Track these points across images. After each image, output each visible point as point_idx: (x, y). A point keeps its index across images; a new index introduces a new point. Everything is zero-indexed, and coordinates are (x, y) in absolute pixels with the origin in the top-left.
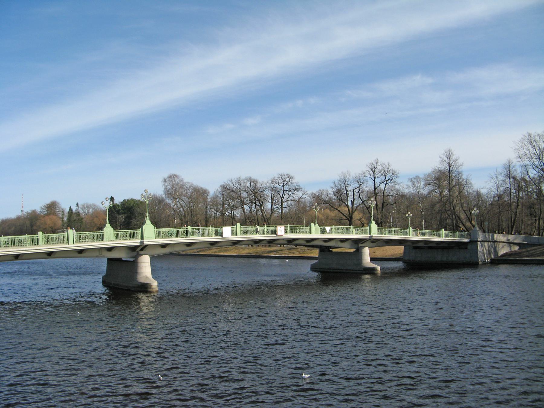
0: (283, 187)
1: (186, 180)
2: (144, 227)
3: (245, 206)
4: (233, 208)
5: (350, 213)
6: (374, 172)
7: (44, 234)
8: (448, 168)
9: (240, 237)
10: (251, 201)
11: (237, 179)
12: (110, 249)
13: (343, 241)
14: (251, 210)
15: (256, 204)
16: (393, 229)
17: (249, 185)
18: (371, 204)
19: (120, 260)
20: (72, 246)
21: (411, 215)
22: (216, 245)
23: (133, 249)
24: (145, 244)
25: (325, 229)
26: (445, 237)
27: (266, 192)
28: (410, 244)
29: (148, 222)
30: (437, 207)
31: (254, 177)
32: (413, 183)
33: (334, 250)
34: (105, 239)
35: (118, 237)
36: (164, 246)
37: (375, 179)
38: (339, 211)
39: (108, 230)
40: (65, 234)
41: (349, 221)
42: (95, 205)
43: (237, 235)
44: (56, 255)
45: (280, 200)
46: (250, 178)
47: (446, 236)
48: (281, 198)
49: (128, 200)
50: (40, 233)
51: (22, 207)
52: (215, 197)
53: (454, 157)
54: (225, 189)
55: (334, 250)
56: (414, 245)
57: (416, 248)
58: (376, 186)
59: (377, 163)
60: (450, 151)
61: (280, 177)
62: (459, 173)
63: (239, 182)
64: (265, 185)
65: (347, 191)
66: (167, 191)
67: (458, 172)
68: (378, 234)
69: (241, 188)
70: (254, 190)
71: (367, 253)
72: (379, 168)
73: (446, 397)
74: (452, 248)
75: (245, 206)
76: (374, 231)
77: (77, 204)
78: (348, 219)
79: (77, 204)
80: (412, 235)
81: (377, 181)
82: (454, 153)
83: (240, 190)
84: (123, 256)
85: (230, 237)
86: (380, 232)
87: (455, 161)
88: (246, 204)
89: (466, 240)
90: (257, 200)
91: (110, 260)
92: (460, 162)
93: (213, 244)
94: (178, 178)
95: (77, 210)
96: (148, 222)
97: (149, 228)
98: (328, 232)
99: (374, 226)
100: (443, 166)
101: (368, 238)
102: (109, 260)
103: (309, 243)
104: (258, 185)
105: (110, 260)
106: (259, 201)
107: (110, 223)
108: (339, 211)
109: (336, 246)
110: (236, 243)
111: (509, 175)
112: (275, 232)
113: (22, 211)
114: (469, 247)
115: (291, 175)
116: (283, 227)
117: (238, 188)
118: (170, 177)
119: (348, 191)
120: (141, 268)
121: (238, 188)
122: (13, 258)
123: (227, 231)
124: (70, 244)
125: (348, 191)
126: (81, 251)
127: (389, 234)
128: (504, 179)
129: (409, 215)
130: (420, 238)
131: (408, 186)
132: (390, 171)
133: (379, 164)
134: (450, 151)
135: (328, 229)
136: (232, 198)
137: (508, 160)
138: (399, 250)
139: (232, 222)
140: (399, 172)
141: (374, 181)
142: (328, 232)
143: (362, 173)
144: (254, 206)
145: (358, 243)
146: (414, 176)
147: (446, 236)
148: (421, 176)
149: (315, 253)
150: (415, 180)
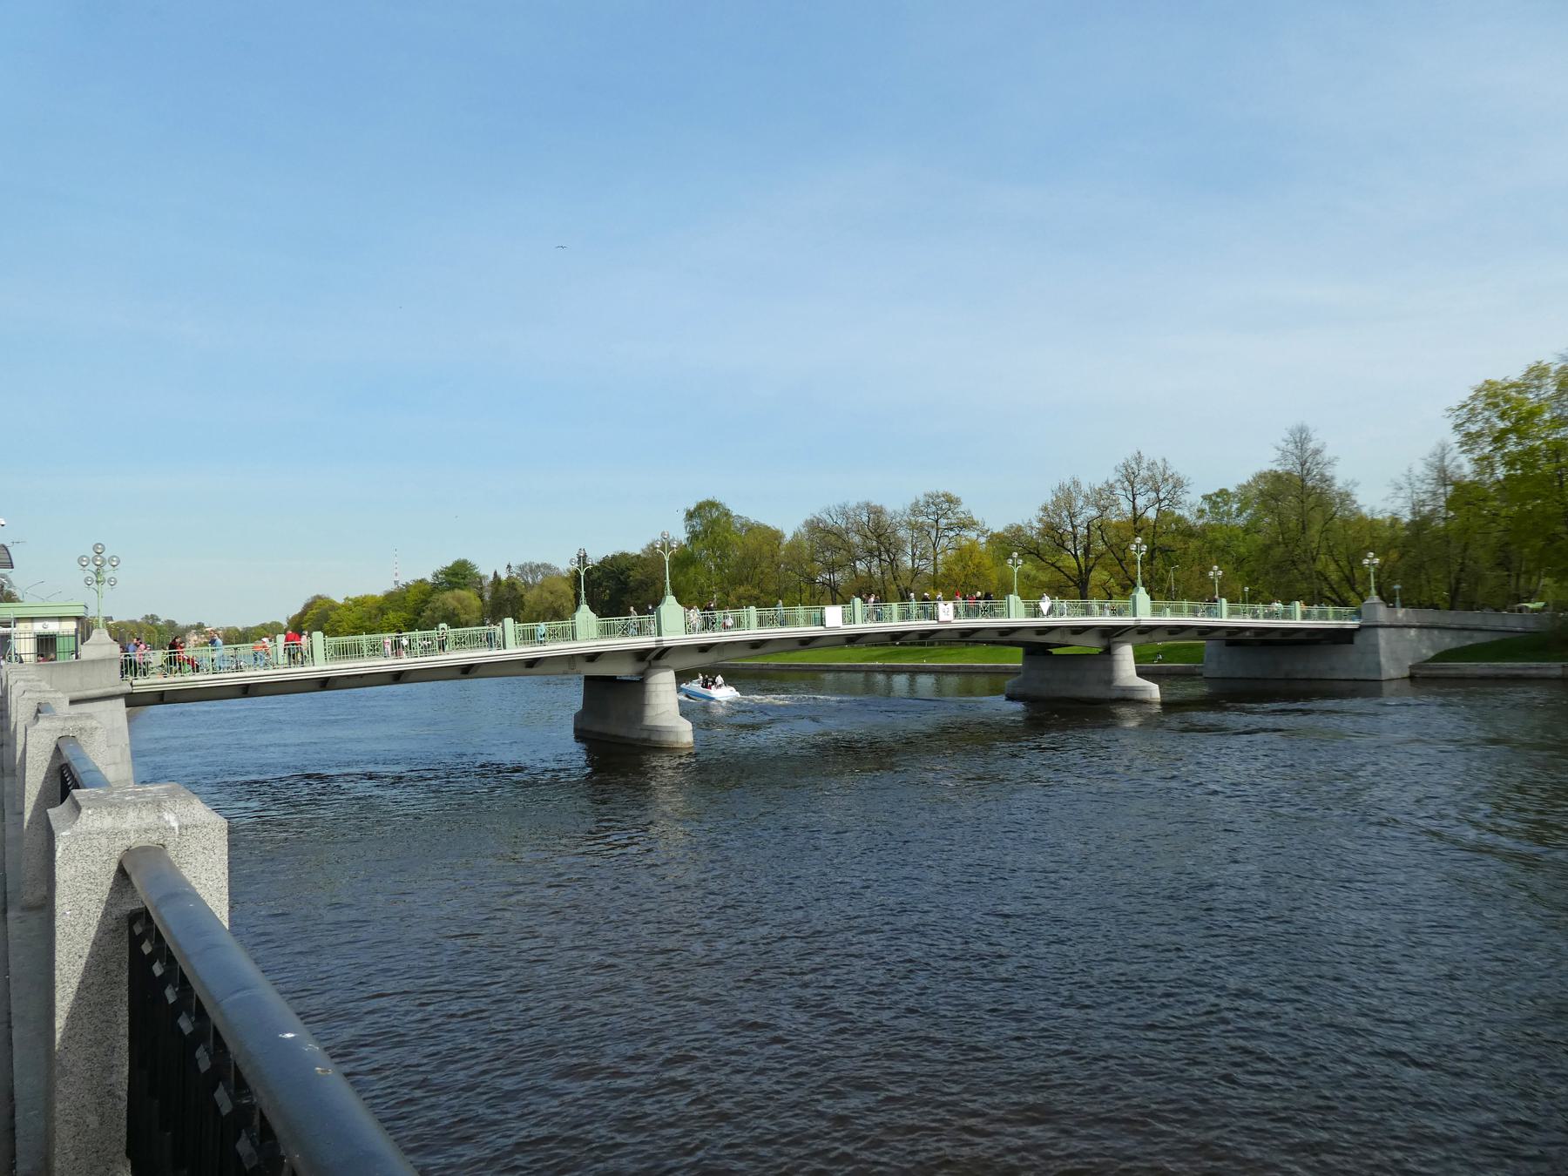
0: (937, 522)
1: (735, 511)
2: (663, 608)
3: (858, 562)
4: (831, 568)
5: (1080, 571)
6: (1132, 484)
7: (519, 622)
8: (1299, 468)
9: (861, 626)
10: (870, 552)
11: (840, 507)
12: (592, 657)
13: (1078, 630)
14: (869, 570)
15: (880, 560)
16: (1185, 603)
17: (865, 519)
18: (1136, 551)
19: (611, 680)
20: (753, 632)
21: (1220, 573)
22: (811, 645)
23: (641, 655)
24: (666, 644)
25: (1038, 606)
26: (1297, 617)
27: (902, 533)
28: (1223, 634)
29: (670, 600)
30: (1278, 552)
31: (876, 502)
32: (1214, 505)
33: (1055, 651)
34: (579, 637)
35: (607, 631)
36: (704, 649)
37: (1134, 499)
38: (1059, 568)
39: (585, 617)
40: (498, 629)
41: (1077, 587)
42: (547, 567)
43: (505, 648)
44: (479, 672)
45: (931, 550)
46: (868, 505)
47: (1305, 616)
48: (934, 545)
49: (614, 557)
50: (509, 621)
51: (396, 574)
52: (795, 545)
53: (1311, 446)
54: (814, 527)
55: (1055, 651)
56: (1234, 638)
57: (1230, 643)
58: (1139, 513)
59: (1138, 464)
60: (1302, 430)
61: (931, 501)
62: (1324, 479)
63: (844, 514)
64: (898, 519)
65: (1074, 527)
66: (694, 537)
67: (1322, 475)
68: (1153, 615)
69: (849, 526)
70: (876, 530)
71: (1126, 658)
72: (1144, 473)
73: (783, 973)
74: (1317, 642)
75: (858, 562)
76: (1143, 609)
77: (509, 566)
78: (1076, 585)
79: (509, 566)
80: (1225, 616)
81: (1141, 501)
82: (1314, 436)
83: (847, 531)
84: (625, 671)
85: (843, 627)
86: (1156, 610)
87: (1317, 452)
88: (859, 560)
89: (1351, 624)
90: (882, 549)
91: (590, 680)
92: (1327, 454)
93: (806, 642)
94: (717, 509)
95: (509, 577)
96: (670, 600)
97: (670, 608)
98: (1045, 613)
99: (1142, 596)
100: (1291, 466)
101: (1132, 623)
102: (588, 679)
103: (1006, 636)
104: (886, 519)
105: (590, 680)
106: (888, 551)
107: (675, 594)
108: (1059, 568)
109: (1063, 641)
110: (852, 640)
111: (1443, 477)
112: (934, 616)
113: (396, 582)
114: (1358, 639)
115: (955, 493)
116: (950, 605)
117: (843, 526)
118: (700, 507)
119: (1076, 527)
120: (657, 696)
121: (843, 526)
122: (458, 673)
123: (834, 617)
124: (582, 641)
125: (1076, 527)
126: (531, 663)
127: (1172, 615)
128: (1430, 488)
129: (1216, 572)
130: (1246, 621)
131: (1201, 511)
132: (1167, 480)
133: (1144, 465)
134: (1302, 430)
135: (1045, 605)
136: (827, 547)
137: (1440, 444)
138: (1013, 659)
139: (837, 596)
140: (1190, 482)
141: (1133, 502)
142: (1045, 613)
143: (1105, 486)
144: (876, 562)
145: (1111, 635)
146: (1216, 491)
147: (1305, 616)
148: (1232, 489)
149: (1013, 659)
150: (1218, 499)
